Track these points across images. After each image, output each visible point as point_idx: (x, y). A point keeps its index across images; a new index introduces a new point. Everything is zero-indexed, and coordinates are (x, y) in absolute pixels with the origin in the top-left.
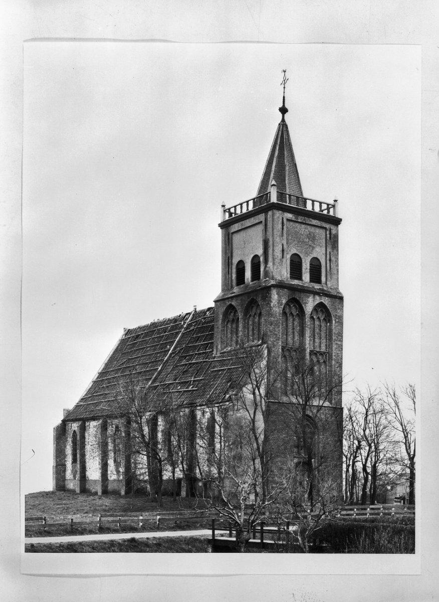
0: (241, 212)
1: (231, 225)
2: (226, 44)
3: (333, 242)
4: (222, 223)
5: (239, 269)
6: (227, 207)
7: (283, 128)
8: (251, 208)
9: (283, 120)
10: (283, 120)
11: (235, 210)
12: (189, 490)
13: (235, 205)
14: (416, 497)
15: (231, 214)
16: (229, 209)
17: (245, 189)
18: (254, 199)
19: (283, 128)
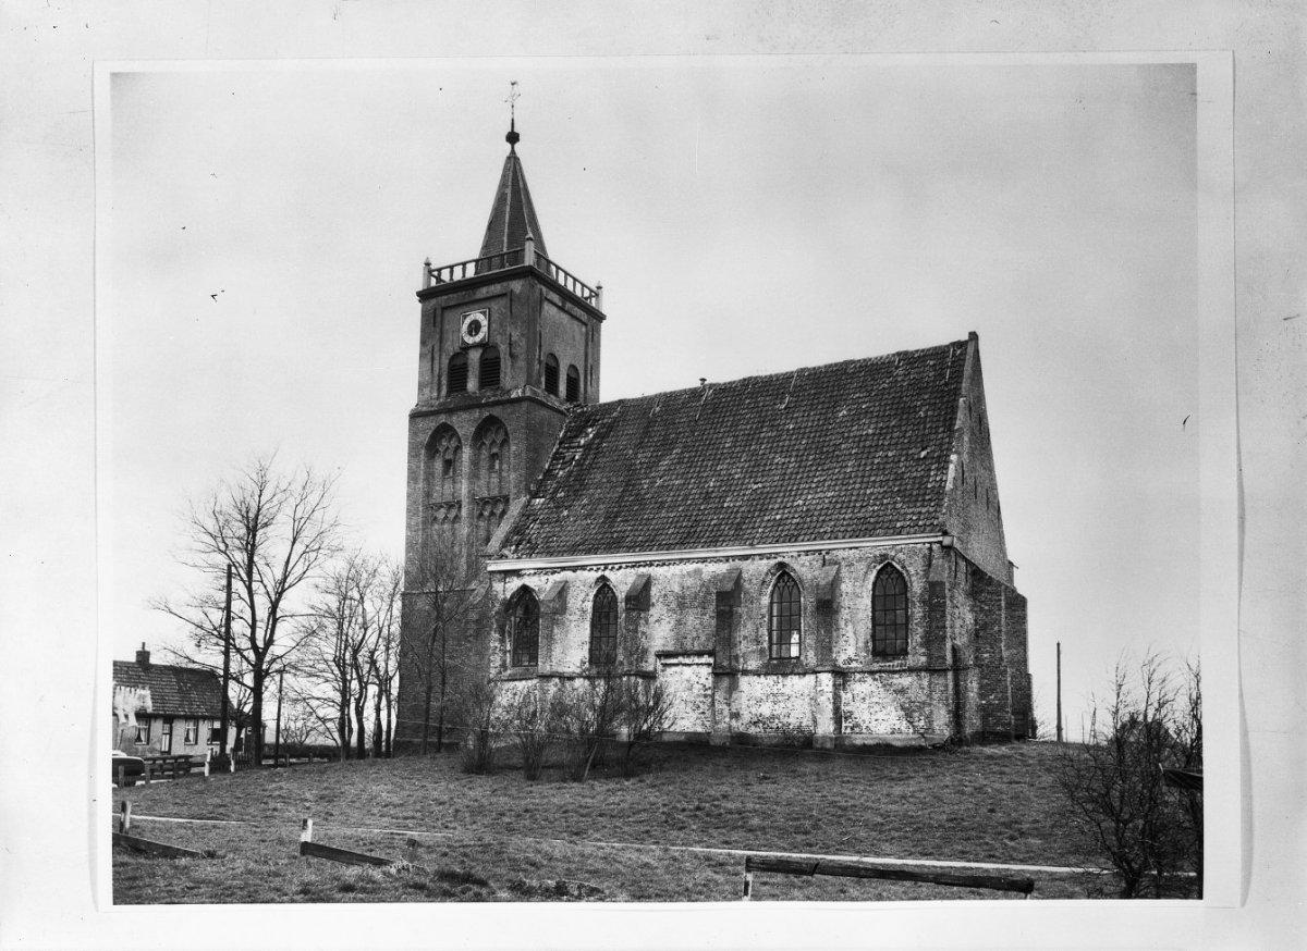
0: (451, 279)
1: (479, 287)
2: (1236, 505)
3: (592, 340)
4: (424, 290)
5: (454, 366)
6: (432, 267)
7: (513, 163)
8: (471, 272)
9: (513, 152)
10: (513, 152)
11: (452, 273)
12: (352, 895)
13: (463, 260)
14: (755, 374)
15: (439, 279)
16: (439, 270)
17: (461, 243)
18: (477, 261)
19: (513, 163)
